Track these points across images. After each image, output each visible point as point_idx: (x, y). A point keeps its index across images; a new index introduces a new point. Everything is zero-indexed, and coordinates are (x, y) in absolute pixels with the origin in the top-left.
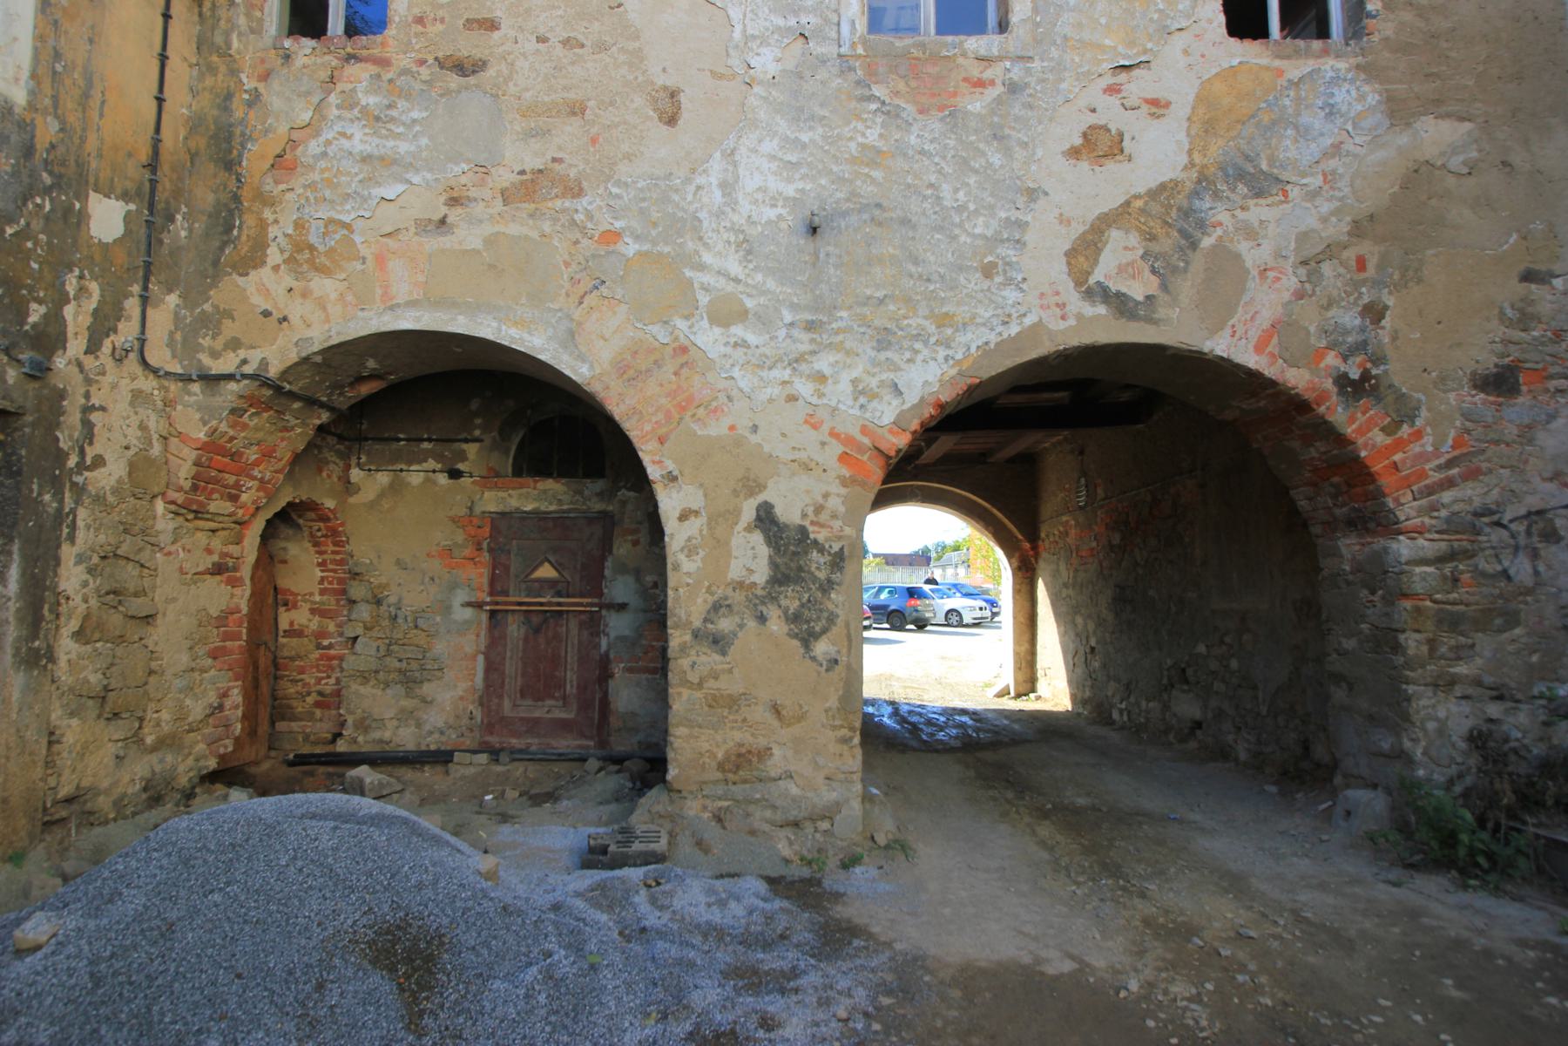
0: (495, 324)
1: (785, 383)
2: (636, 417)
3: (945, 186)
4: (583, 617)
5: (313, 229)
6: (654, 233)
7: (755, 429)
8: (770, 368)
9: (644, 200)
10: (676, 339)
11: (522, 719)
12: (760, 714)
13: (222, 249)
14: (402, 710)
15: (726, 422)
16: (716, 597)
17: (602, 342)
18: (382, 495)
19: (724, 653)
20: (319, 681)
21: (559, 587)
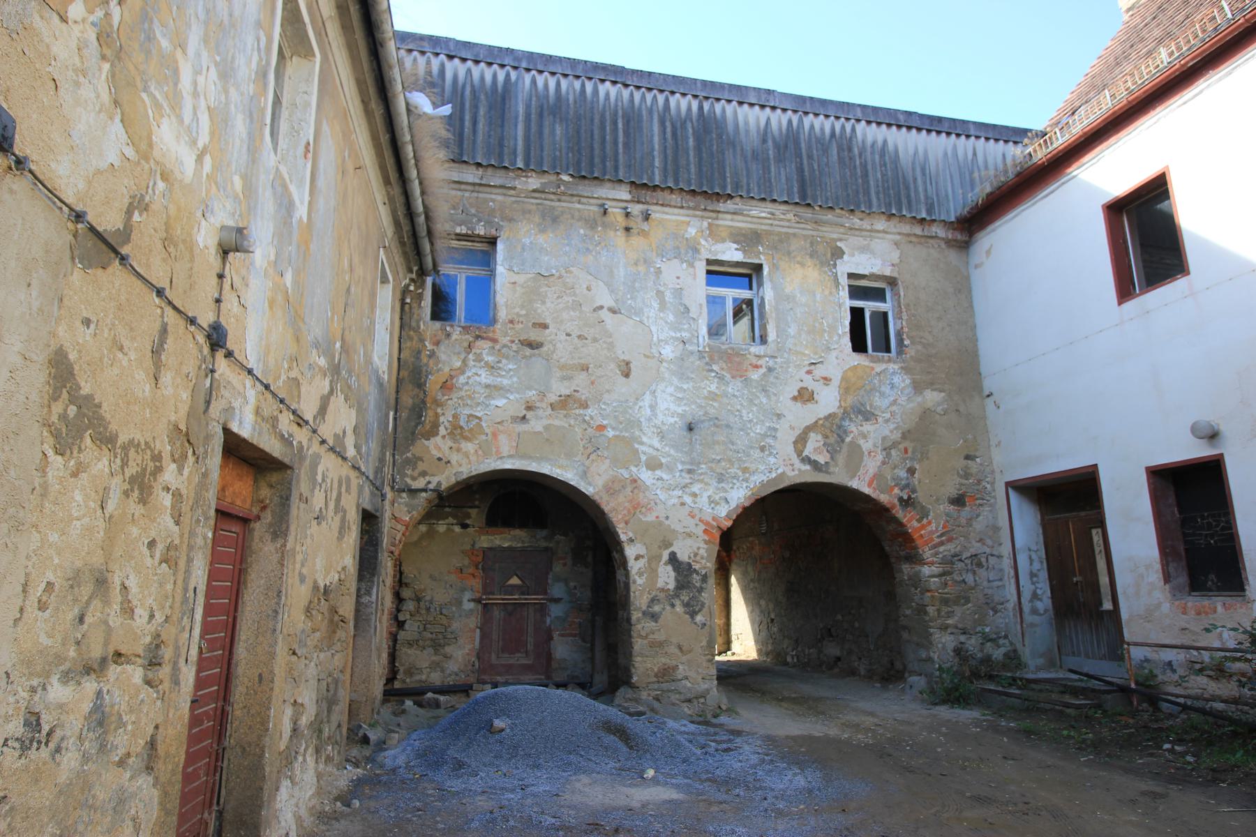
7: (667, 518)
12: (673, 650)
13: (416, 427)
14: (433, 662)
15: (655, 514)
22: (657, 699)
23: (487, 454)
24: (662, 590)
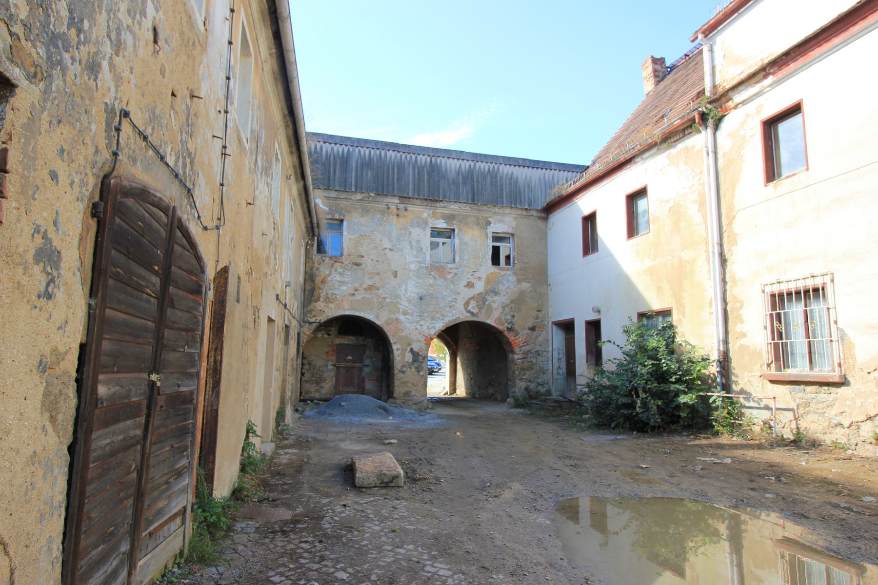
12: (410, 385)
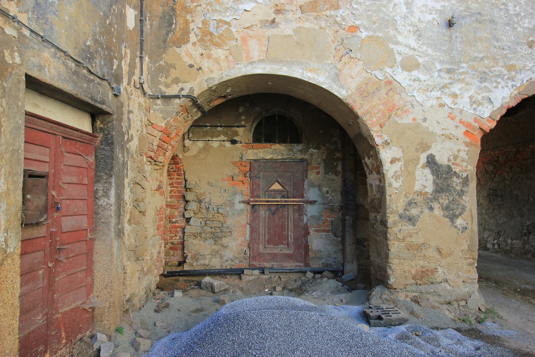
0: (301, 71)
1: (438, 98)
2: (369, 115)
3: (510, 4)
4: (295, 207)
5: (211, 25)
6: (374, 27)
7: (425, 120)
8: (431, 91)
9: (369, 11)
10: (386, 77)
11: (268, 254)
12: (432, 253)
13: (167, 34)
14: (213, 251)
15: (411, 116)
16: (409, 199)
17: (351, 79)
18: (200, 152)
19: (414, 225)
20: (171, 238)
21: (284, 193)
22: (416, 301)
23: (237, 61)
24: (420, 193)
